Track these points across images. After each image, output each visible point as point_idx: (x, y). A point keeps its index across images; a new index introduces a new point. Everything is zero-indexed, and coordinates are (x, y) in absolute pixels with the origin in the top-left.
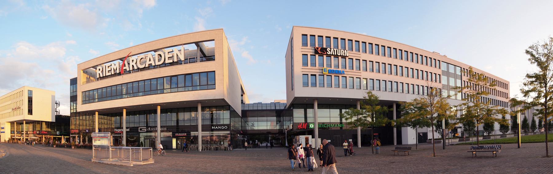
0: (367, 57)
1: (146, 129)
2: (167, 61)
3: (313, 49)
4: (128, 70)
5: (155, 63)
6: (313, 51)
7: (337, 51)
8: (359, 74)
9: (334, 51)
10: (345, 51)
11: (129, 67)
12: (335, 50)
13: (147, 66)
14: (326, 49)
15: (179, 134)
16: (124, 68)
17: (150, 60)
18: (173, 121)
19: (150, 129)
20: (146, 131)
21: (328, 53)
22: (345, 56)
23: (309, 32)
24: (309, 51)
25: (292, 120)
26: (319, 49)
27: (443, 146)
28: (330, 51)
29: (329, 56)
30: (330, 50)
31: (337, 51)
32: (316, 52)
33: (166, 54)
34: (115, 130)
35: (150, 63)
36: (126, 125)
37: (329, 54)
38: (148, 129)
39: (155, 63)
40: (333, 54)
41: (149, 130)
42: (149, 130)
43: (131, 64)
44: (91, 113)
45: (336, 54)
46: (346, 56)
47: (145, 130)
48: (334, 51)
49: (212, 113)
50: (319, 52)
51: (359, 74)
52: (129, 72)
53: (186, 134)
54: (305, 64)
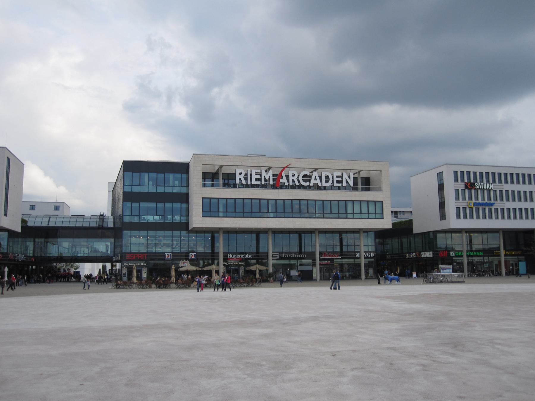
0: (509, 187)
1: (278, 256)
2: (336, 184)
3: (463, 184)
4: (286, 184)
5: (378, 214)
6: (464, 186)
7: (483, 185)
8: (503, 205)
9: (481, 185)
10: (490, 184)
11: (288, 180)
12: (482, 184)
13: (312, 184)
14: (474, 184)
15: (322, 262)
16: (281, 181)
17: (316, 179)
18: (311, 245)
19: (284, 256)
20: (278, 258)
21: (476, 187)
22: (490, 189)
23: (459, 169)
24: (461, 186)
25: (59, 254)
26: (469, 185)
27: (234, 203)
28: (478, 185)
29: (477, 190)
30: (477, 184)
31: (483, 185)
32: (466, 187)
33: (335, 177)
34: (228, 256)
35: (316, 182)
36: (223, 250)
37: (477, 188)
38: (282, 255)
39: (378, 214)
40: (481, 188)
41: (293, 256)
42: (283, 256)
43: (291, 178)
44: (213, 232)
45: (482, 188)
46: (492, 189)
47: (277, 257)
48: (481, 185)
49: (402, 243)
50: (469, 187)
51: (503, 205)
52: (287, 187)
53: (329, 262)
54: (457, 198)
